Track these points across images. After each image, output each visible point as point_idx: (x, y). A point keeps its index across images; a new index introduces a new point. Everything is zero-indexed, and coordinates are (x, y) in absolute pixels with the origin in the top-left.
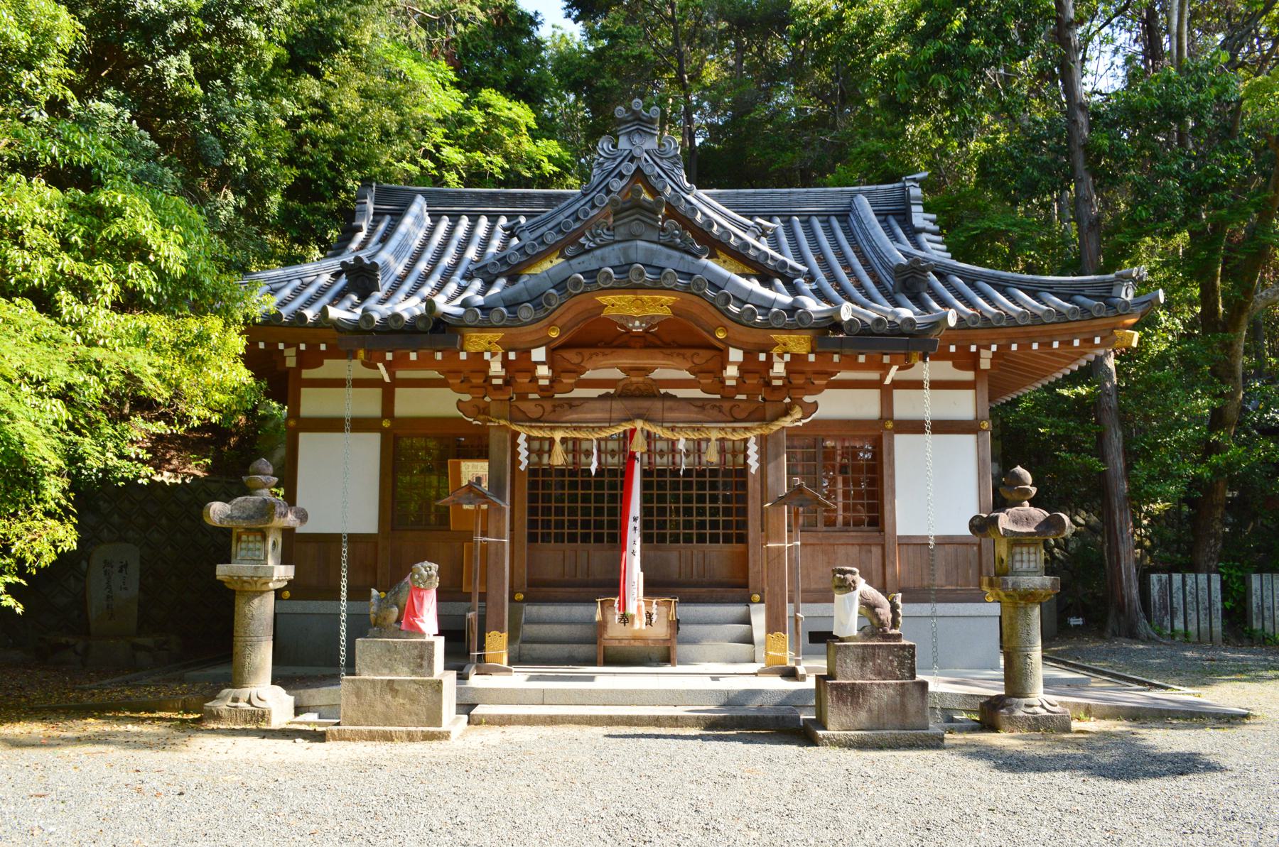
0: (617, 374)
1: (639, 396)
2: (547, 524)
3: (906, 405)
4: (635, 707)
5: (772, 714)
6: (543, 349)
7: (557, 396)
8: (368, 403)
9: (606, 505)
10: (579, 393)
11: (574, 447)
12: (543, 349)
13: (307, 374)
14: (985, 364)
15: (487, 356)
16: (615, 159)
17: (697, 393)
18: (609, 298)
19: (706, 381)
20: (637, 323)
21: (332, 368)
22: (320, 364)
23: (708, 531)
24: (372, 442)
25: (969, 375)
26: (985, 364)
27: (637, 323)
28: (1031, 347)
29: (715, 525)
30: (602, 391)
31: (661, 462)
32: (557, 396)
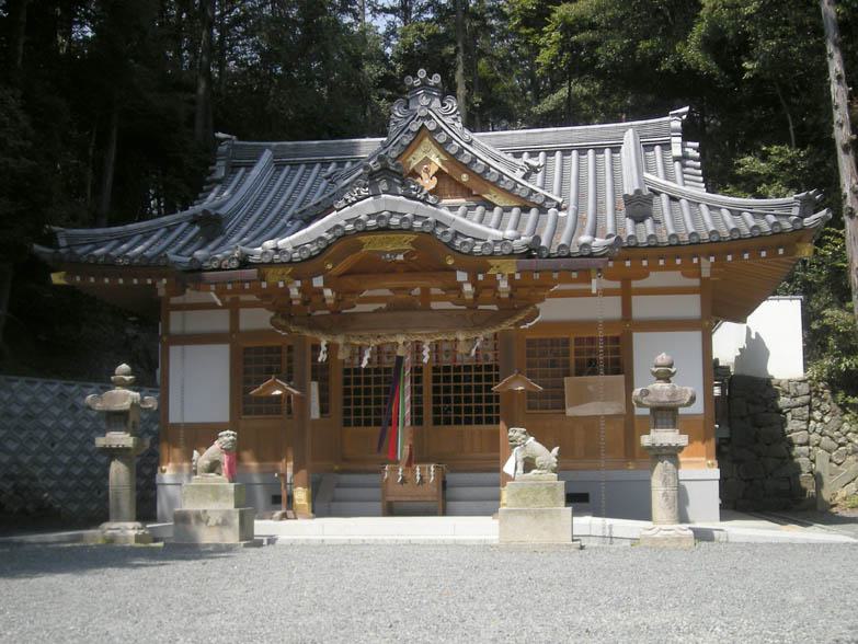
0: (386, 292)
1: (403, 310)
2: (358, 412)
3: (643, 308)
4: (342, 537)
5: (158, 481)
6: (321, 278)
7: (480, 307)
8: (219, 321)
9: (373, 396)
10: (360, 308)
11: (331, 348)
12: (321, 278)
13: (174, 300)
14: (706, 273)
15: (499, 277)
16: (406, 118)
17: (447, 305)
18: (366, 237)
19: (454, 296)
20: (388, 256)
21: (656, 279)
22: (647, 275)
23: (463, 415)
24: (222, 353)
25: (696, 282)
26: (706, 273)
27: (388, 256)
28: (726, 259)
29: (447, 400)
30: (377, 306)
31: (446, 361)
32: (480, 307)
